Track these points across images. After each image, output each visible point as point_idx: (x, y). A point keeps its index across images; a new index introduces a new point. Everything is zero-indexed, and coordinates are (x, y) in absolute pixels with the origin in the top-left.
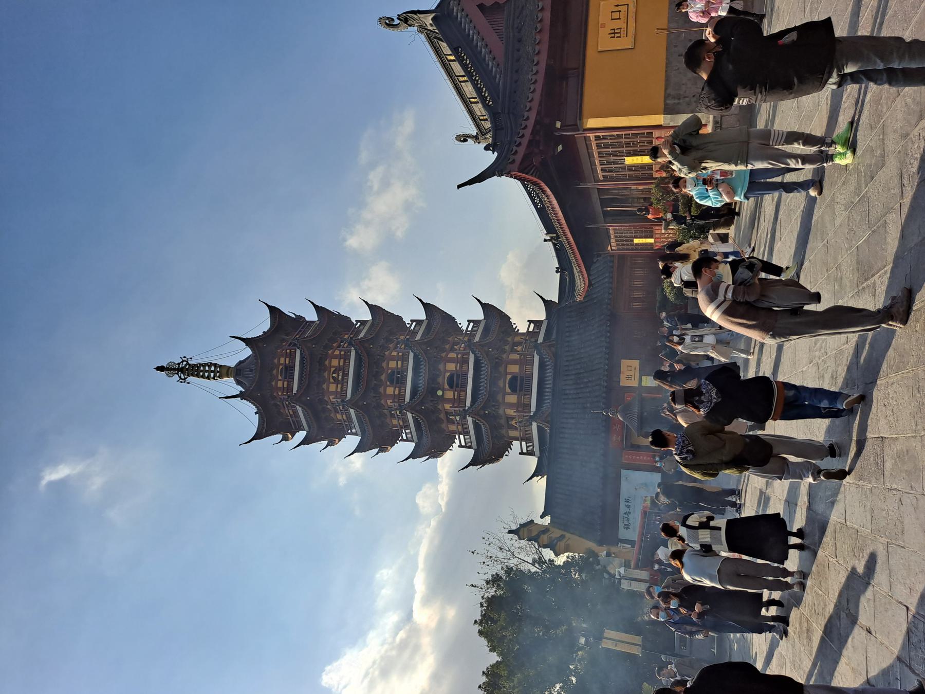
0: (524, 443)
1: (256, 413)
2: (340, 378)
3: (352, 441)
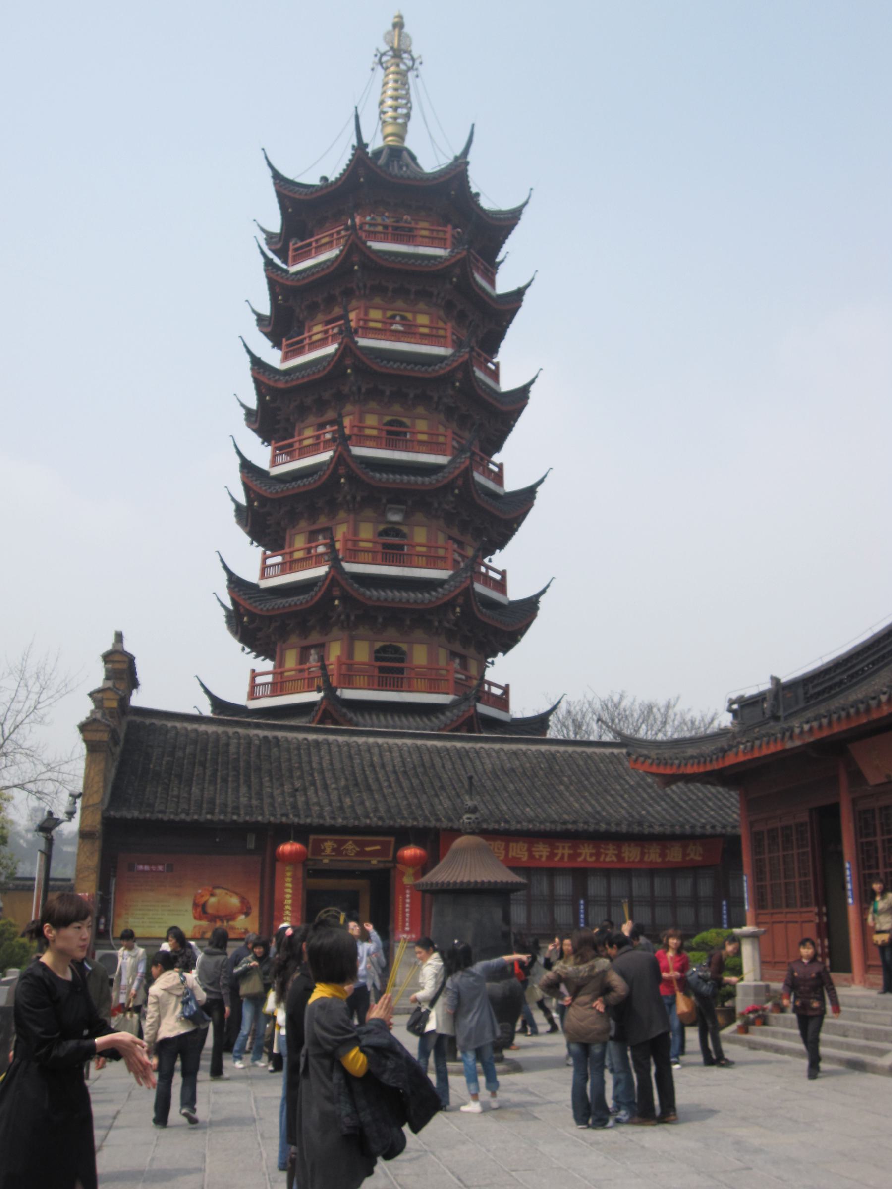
0: (269, 678)
1: (324, 179)
2: (394, 327)
3: (261, 455)
